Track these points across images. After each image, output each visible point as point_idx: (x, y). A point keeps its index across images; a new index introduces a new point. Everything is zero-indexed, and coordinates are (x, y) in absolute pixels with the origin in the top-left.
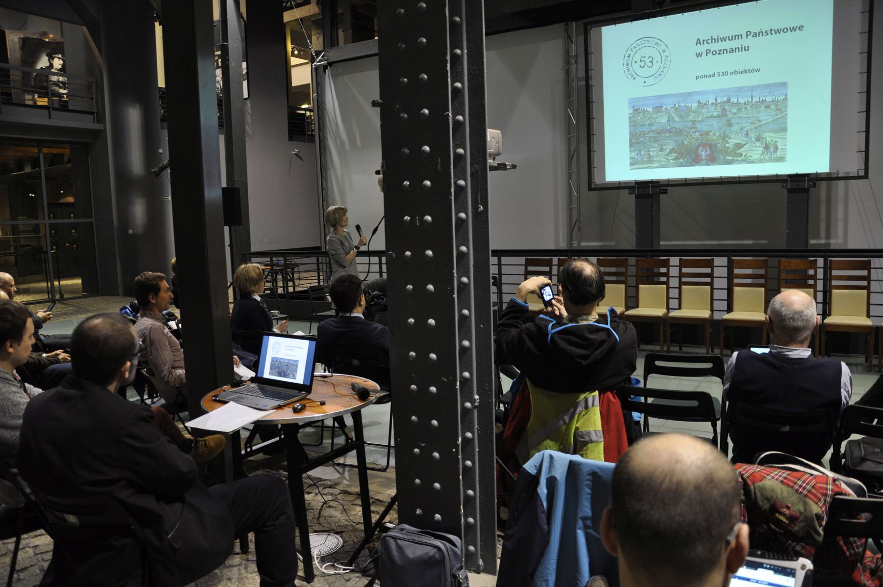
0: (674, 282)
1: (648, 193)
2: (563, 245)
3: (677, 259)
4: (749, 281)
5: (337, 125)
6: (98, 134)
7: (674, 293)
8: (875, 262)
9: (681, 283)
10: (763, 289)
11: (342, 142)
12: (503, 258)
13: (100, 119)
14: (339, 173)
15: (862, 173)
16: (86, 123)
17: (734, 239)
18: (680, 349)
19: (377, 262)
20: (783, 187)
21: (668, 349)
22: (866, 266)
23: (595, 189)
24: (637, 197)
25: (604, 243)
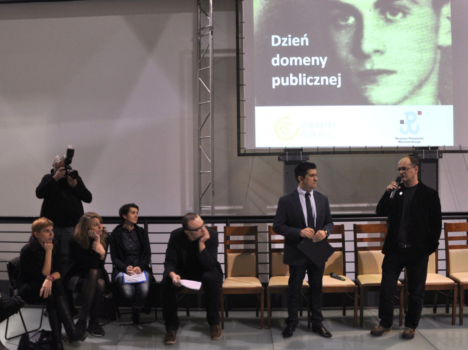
23: (245, 155)
25: (232, 207)
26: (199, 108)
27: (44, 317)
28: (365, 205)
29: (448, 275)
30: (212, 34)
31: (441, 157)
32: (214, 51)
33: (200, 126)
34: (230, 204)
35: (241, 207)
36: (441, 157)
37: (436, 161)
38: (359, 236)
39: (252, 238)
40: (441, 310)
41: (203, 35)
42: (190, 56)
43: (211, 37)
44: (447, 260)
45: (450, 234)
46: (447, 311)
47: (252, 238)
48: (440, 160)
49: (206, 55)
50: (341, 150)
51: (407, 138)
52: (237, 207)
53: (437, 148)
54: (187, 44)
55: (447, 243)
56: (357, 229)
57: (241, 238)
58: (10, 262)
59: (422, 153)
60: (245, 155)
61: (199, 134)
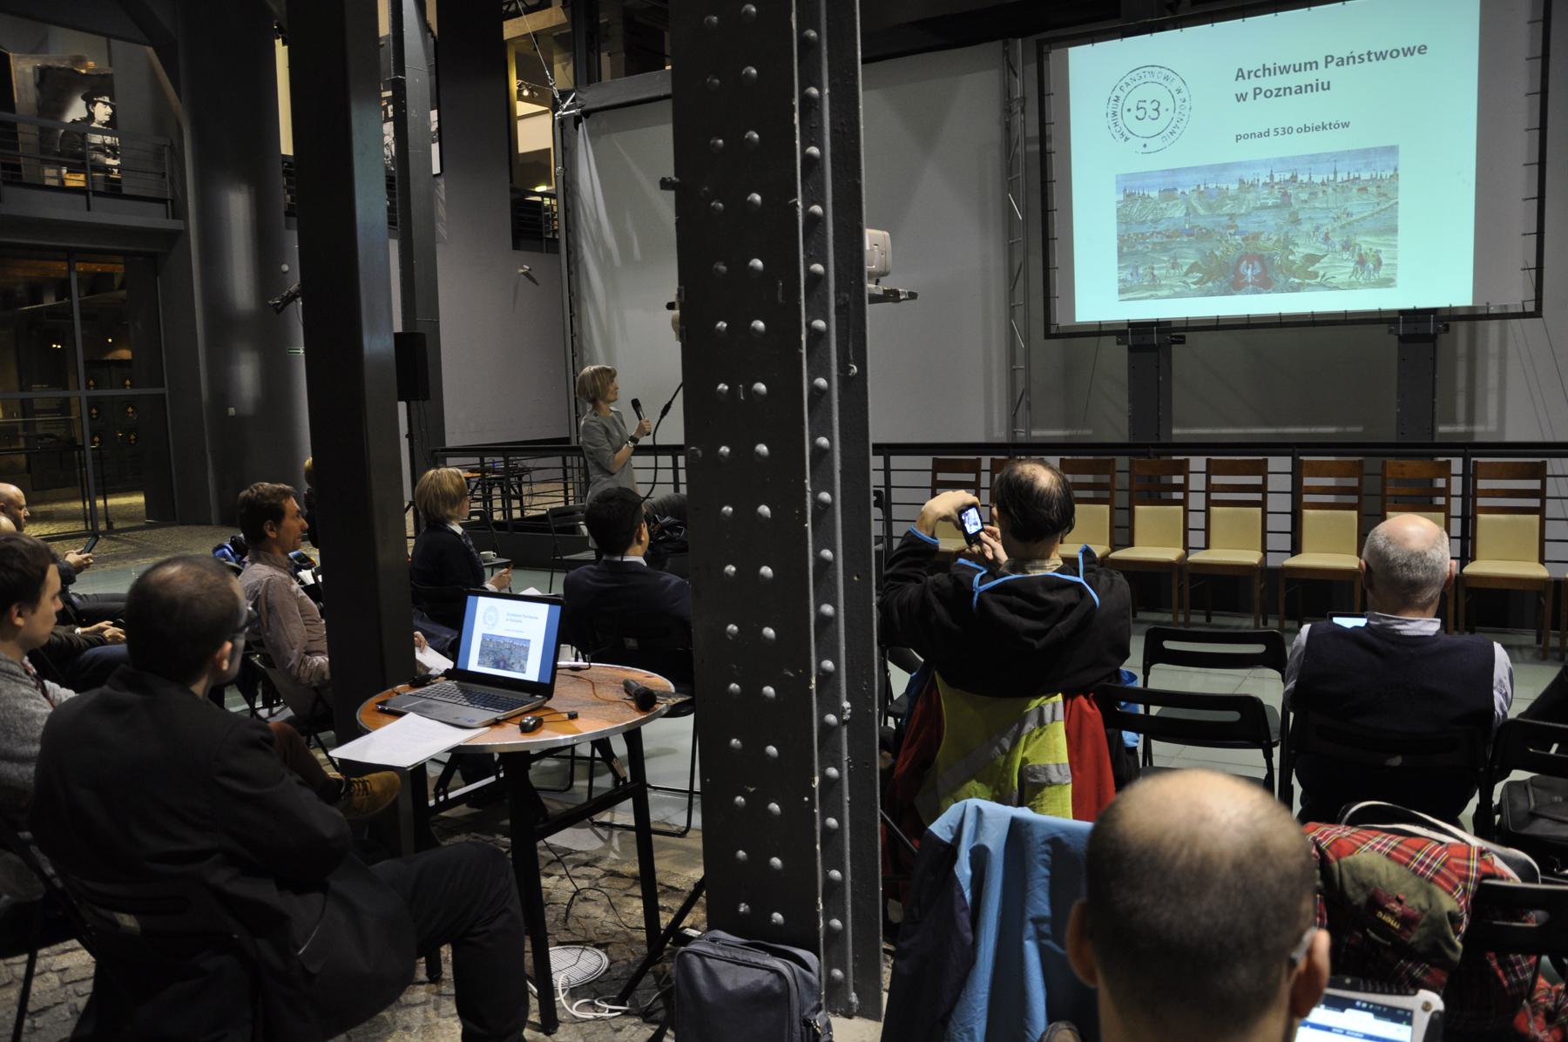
0: (1197, 501)
1: (1150, 343)
2: (1000, 436)
3: (1203, 459)
4: (1330, 499)
5: (598, 222)
6: (174, 238)
7: (1197, 520)
8: (1554, 465)
9: (1210, 503)
10: (1355, 513)
11: (608, 253)
12: (892, 458)
13: (178, 211)
14: (602, 307)
15: (1530, 307)
16: (152, 218)
17: (1304, 424)
18: (1208, 620)
19: (670, 465)
20: (1391, 331)
21: (1187, 619)
23: (1056, 336)
24: (1130, 349)
34: (1066, 427)
35: (1088, 432)
38: (1215, 480)
39: (1106, 479)
47: (1106, 479)
50: (1056, 202)
51: (1313, 65)
56: (1211, 470)
57: (1330, 482)
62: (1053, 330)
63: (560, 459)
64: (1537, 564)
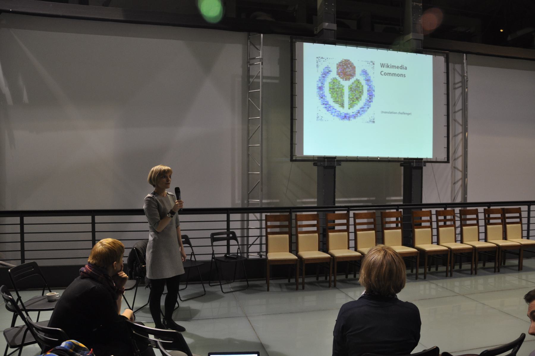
1: (328, 165)
2: (238, 204)
4: (277, 230)
9: (356, 231)
10: (374, 232)
12: (96, 217)
15: (446, 160)
17: (357, 197)
18: (317, 279)
21: (303, 280)
22: (289, 219)
23: (296, 160)
25: (271, 201)
26: (247, 121)
27: (506, 264)
28: (366, 199)
29: (356, 250)
30: (262, 64)
31: (425, 166)
32: (263, 77)
33: (248, 138)
34: (268, 198)
35: (278, 201)
36: (425, 166)
37: (422, 168)
40: (322, 279)
41: (253, 64)
42: (240, 79)
43: (261, 66)
44: (438, 235)
45: (358, 221)
46: (326, 279)
48: (424, 168)
49: (256, 80)
52: (274, 201)
53: (422, 159)
54: (238, 69)
55: (437, 224)
58: (133, 250)
59: (413, 162)
60: (296, 160)
61: (248, 143)
62: (294, 158)
63: (19, 218)
64: (288, 253)
